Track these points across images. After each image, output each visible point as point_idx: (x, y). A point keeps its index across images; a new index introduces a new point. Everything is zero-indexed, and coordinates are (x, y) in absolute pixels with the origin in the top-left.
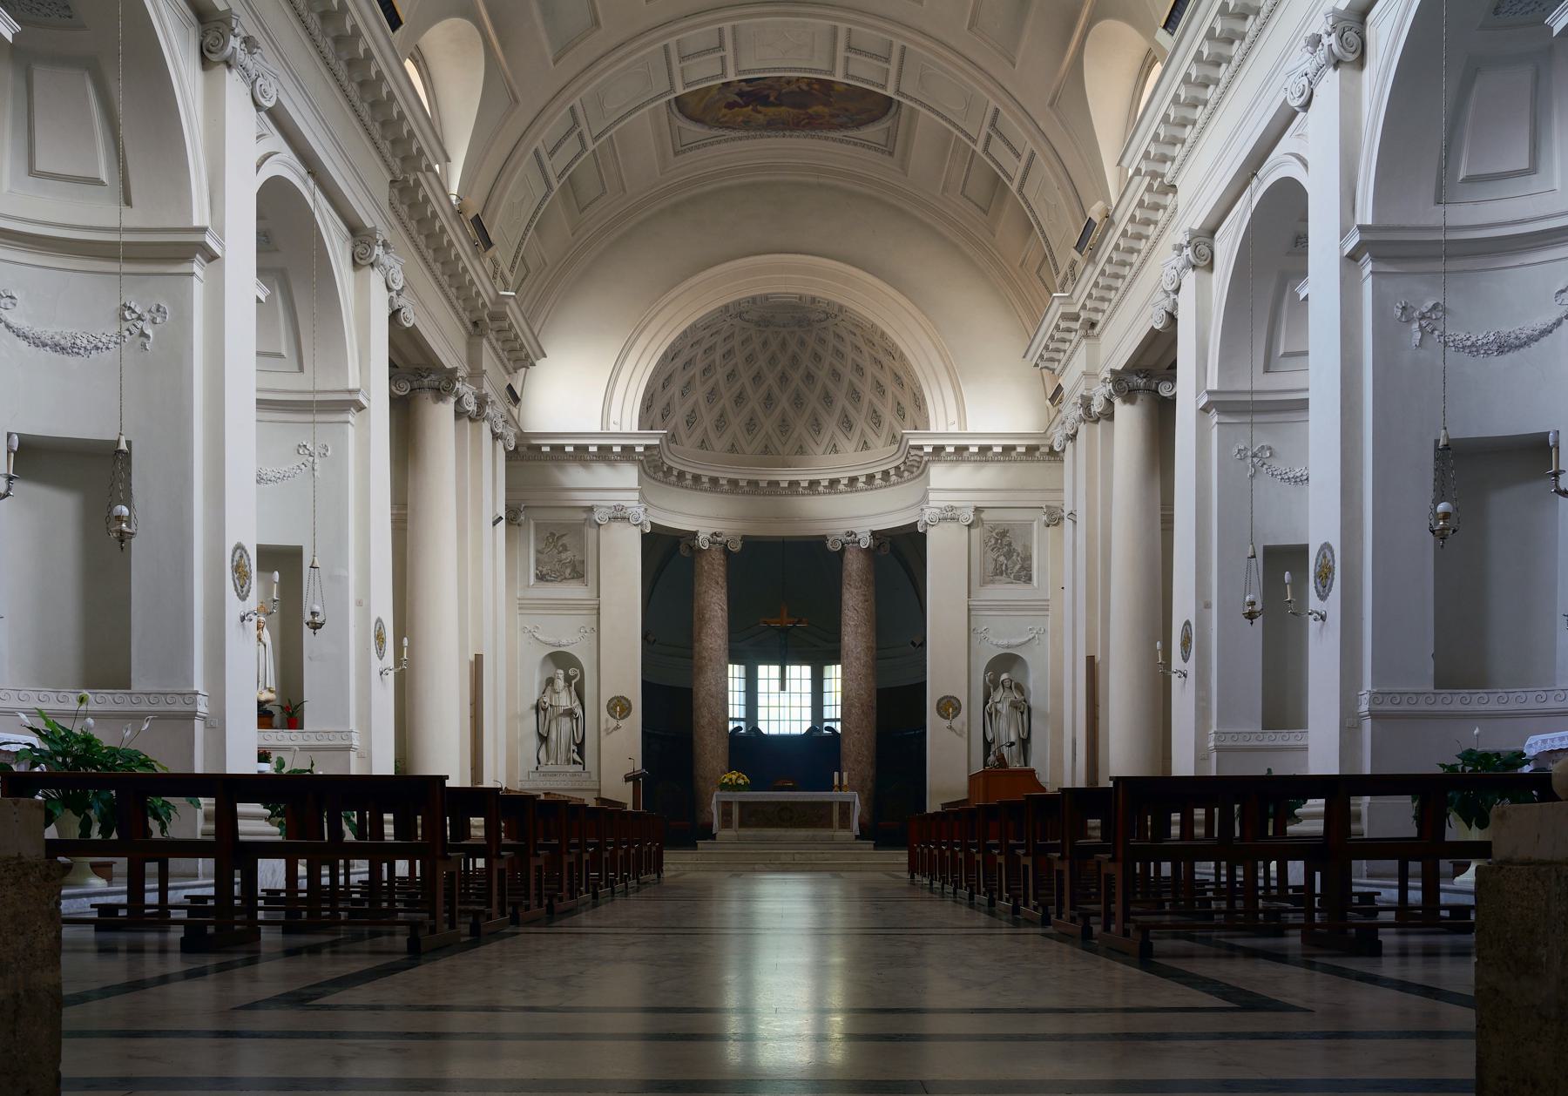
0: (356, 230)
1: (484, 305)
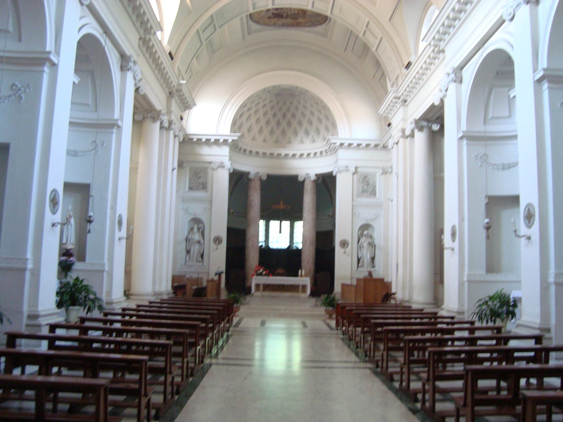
0: (124, 58)
1: (174, 86)
